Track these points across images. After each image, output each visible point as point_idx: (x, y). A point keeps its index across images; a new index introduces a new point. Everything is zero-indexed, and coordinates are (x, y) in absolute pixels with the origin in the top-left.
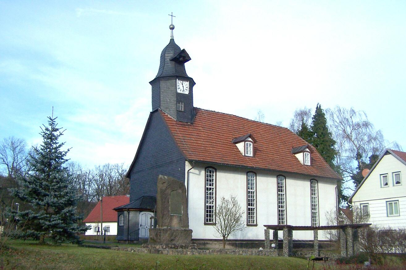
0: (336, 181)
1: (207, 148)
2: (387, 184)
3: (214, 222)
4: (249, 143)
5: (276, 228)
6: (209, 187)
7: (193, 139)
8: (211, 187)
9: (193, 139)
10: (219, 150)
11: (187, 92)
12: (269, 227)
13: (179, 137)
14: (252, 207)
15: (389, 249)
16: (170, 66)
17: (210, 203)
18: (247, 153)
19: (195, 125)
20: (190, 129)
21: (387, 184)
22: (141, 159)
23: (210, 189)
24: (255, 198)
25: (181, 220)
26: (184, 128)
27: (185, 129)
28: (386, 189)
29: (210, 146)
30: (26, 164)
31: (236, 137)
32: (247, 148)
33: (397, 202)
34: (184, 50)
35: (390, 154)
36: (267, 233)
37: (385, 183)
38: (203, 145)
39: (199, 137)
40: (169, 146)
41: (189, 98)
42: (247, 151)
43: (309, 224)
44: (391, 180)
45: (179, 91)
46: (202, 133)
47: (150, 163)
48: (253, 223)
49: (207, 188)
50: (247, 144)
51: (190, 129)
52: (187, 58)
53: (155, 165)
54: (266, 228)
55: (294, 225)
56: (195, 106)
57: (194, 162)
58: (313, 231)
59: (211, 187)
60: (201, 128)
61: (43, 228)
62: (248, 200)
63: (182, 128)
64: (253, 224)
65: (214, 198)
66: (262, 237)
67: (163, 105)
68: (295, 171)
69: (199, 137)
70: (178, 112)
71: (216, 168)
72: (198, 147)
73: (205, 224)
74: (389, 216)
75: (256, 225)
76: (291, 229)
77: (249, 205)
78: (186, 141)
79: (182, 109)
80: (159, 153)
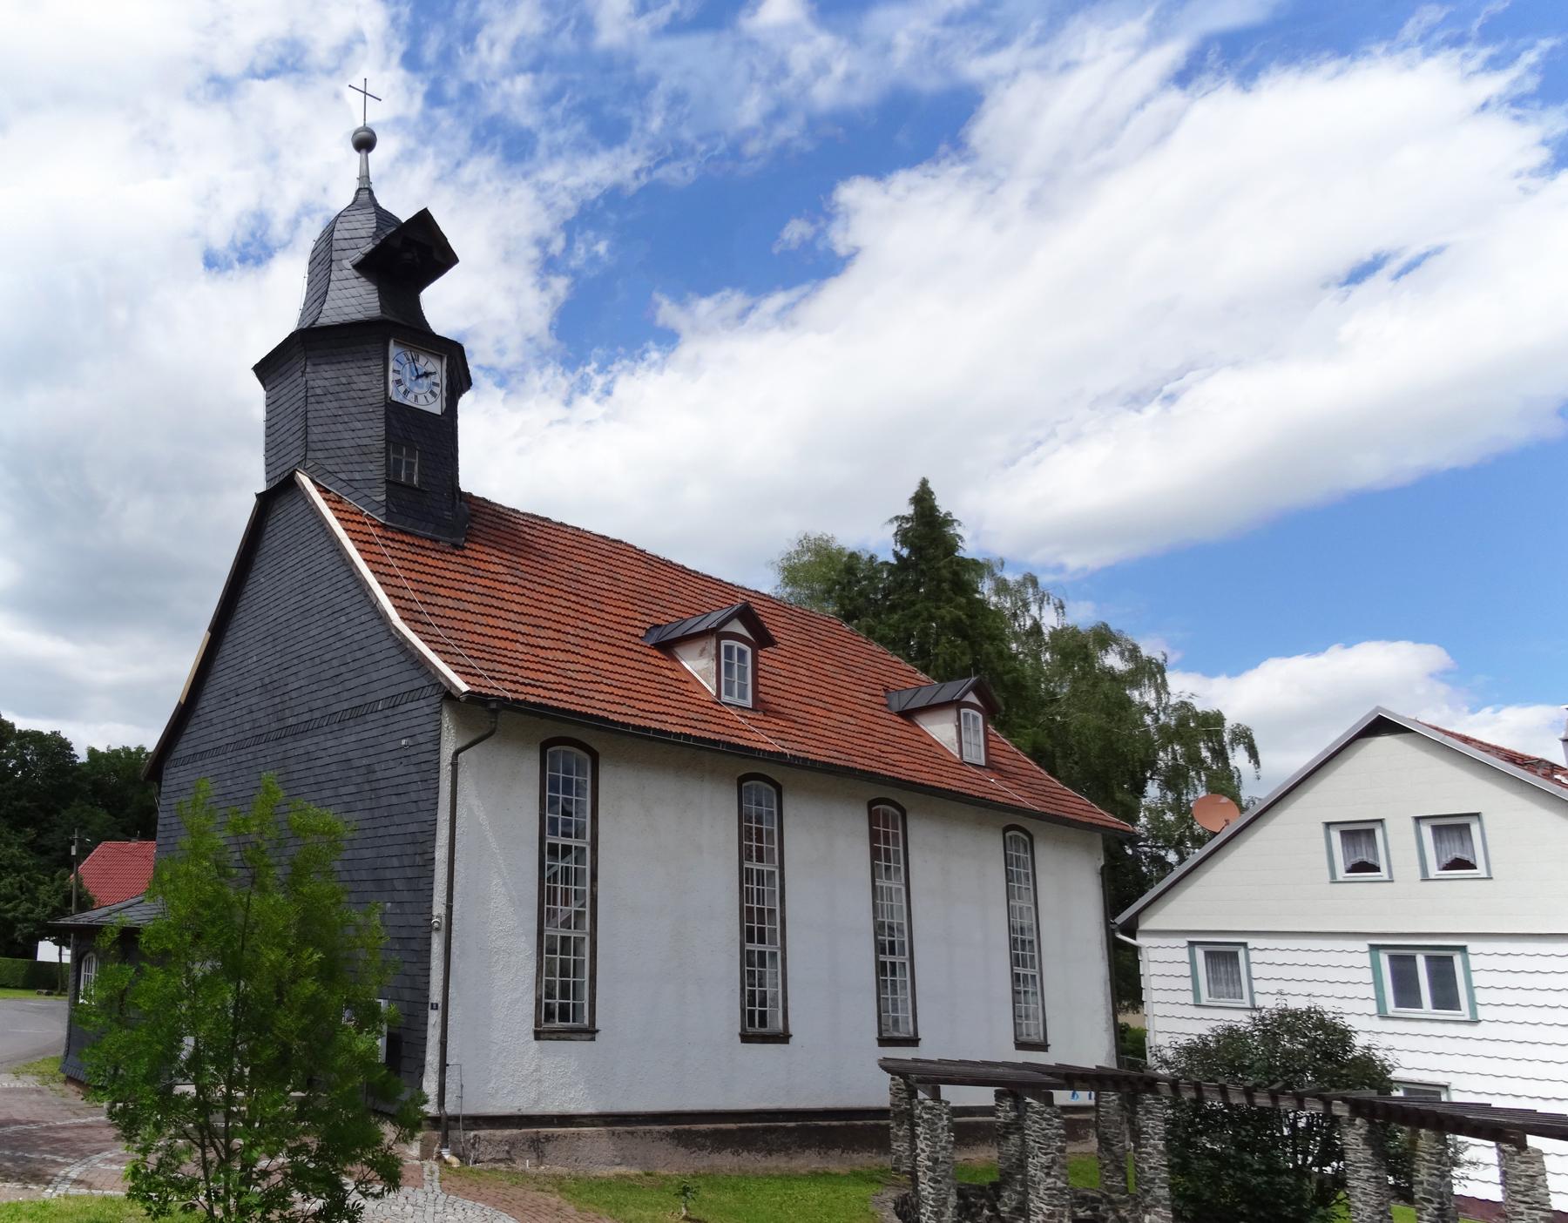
0: (1098, 839)
3: (586, 1022)
4: (737, 644)
6: (561, 841)
8: (572, 842)
10: (601, 665)
11: (436, 407)
14: (761, 947)
16: (355, 299)
17: (566, 924)
18: (729, 692)
19: (467, 552)
22: (207, 702)
23: (567, 849)
26: (420, 559)
28: (1363, 890)
31: (657, 621)
32: (729, 666)
34: (424, 219)
38: (521, 638)
40: (352, 451)
41: (437, 437)
42: (729, 685)
45: (396, 395)
47: (248, 717)
49: (553, 849)
50: (729, 649)
53: (274, 726)
56: (465, 486)
59: (572, 842)
61: (1192, 773)
62: (746, 914)
65: (1192, 860)
71: (595, 746)
73: (538, 1035)
74: (1390, 1013)
77: (751, 940)
78: (436, 610)
79: (410, 476)
80: (294, 670)
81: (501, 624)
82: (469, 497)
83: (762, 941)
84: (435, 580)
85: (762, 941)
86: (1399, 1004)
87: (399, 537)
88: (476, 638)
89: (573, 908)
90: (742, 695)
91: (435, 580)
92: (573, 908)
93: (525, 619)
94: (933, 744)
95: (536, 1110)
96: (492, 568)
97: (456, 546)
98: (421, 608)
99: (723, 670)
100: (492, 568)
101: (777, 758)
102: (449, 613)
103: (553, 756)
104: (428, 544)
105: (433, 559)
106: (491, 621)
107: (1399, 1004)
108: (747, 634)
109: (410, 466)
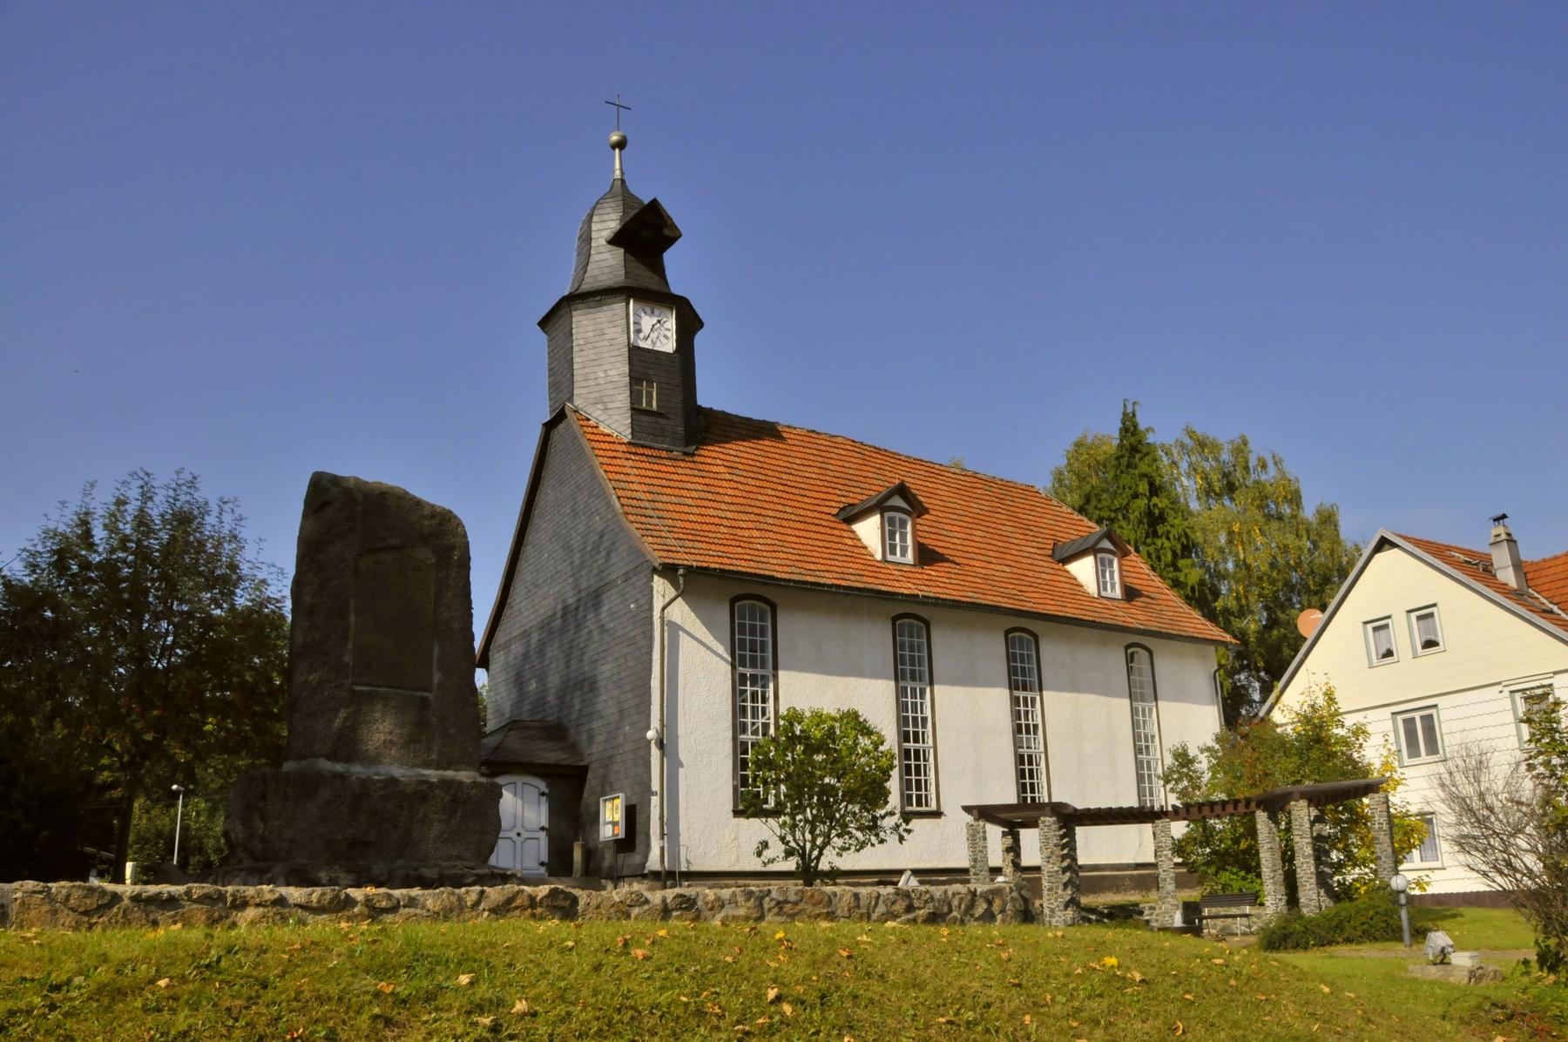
1: (740, 533)
2: (1389, 653)
4: (898, 515)
5: (1013, 819)
7: (690, 502)
9: (690, 502)
12: (985, 813)
13: (635, 495)
15: (1233, 982)
18: (893, 552)
20: (680, 471)
21: (1389, 653)
24: (928, 713)
25: (422, 723)
26: (655, 467)
27: (663, 468)
28: (1388, 669)
29: (751, 525)
30: (791, 865)
33: (1433, 711)
34: (654, 204)
35: (1394, 545)
36: (976, 841)
37: (1383, 650)
38: (725, 522)
39: (710, 496)
43: (1130, 801)
44: (1403, 635)
46: (725, 484)
48: (919, 804)
51: (680, 471)
52: (667, 232)
54: (969, 818)
55: (1080, 804)
57: (681, 571)
58: (1149, 826)
59: (759, 672)
60: (722, 469)
63: (648, 466)
64: (923, 809)
66: (959, 857)
67: (584, 391)
68: (1070, 612)
69: (710, 496)
70: (636, 411)
72: (705, 527)
75: (937, 814)
76: (1070, 819)
79: (649, 403)
81: (712, 512)
82: (709, 412)
83: (917, 741)
84: (664, 483)
85: (917, 741)
86: (1410, 757)
87: (641, 451)
88: (688, 525)
89: (761, 720)
90: (903, 554)
91: (664, 483)
92: (761, 720)
93: (732, 508)
94: (1072, 580)
95: (737, 868)
96: (714, 469)
97: (685, 454)
98: (647, 504)
99: (888, 535)
100: (714, 469)
101: (926, 601)
102: (671, 507)
103: (742, 608)
104: (664, 454)
105: (667, 467)
106: (703, 511)
107: (1410, 757)
108: (905, 506)
109: (649, 395)
